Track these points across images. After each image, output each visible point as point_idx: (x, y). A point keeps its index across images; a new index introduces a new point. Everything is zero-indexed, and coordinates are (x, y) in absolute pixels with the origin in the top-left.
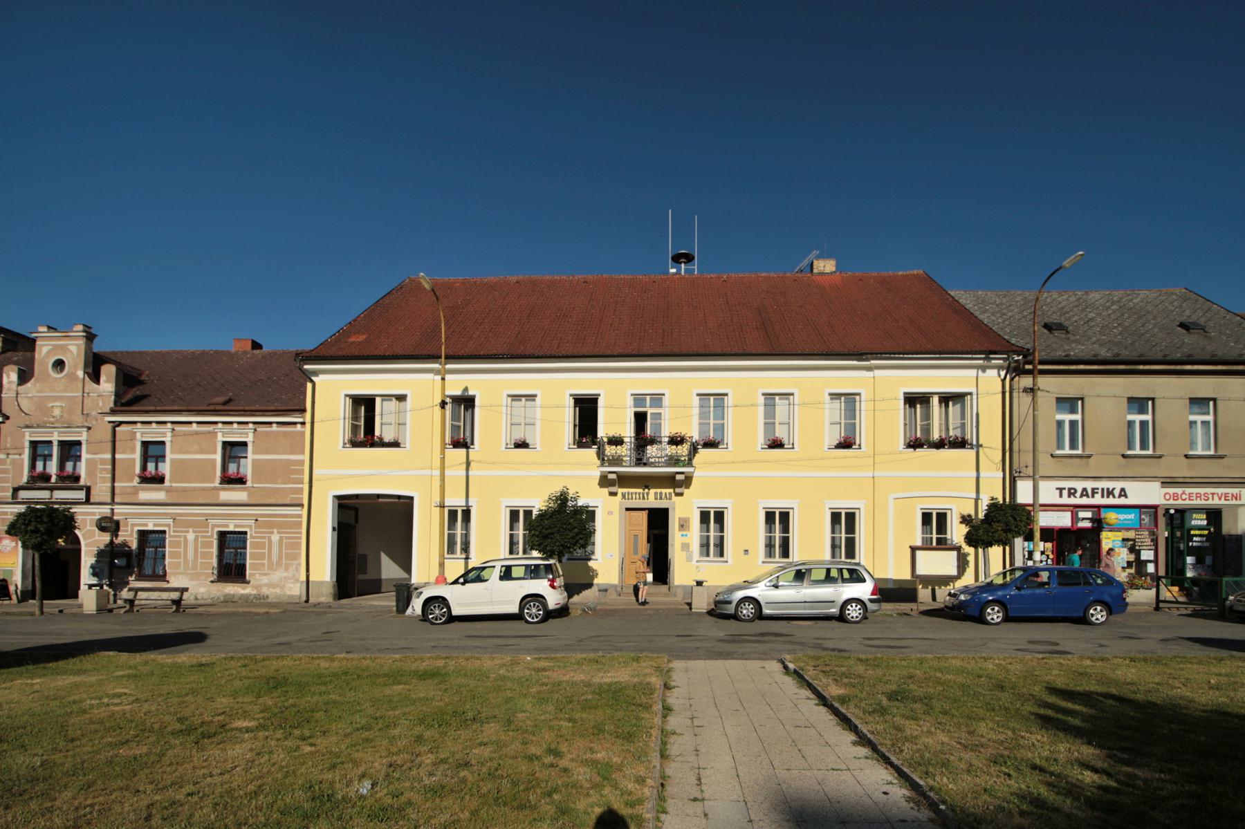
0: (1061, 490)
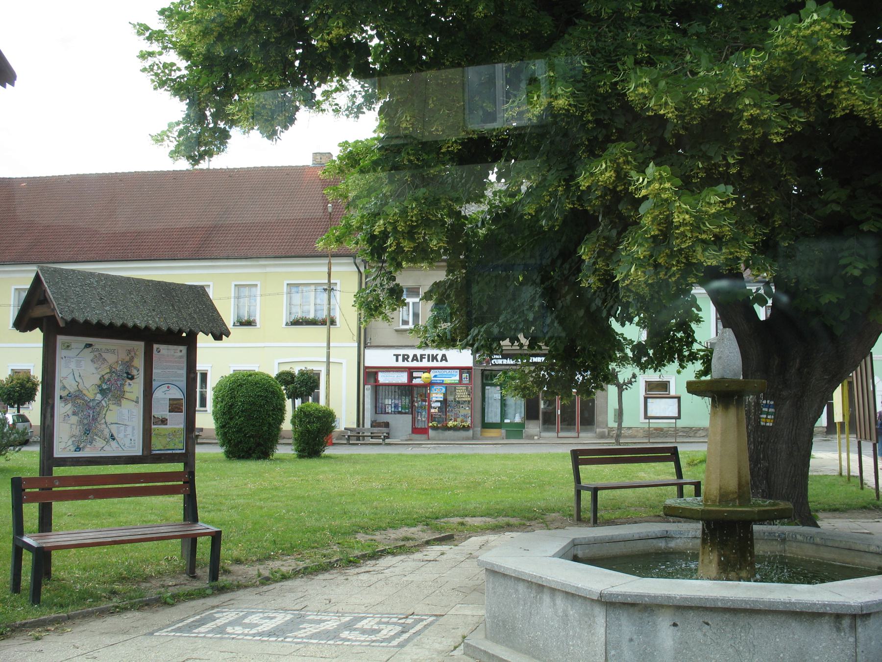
0: (397, 356)
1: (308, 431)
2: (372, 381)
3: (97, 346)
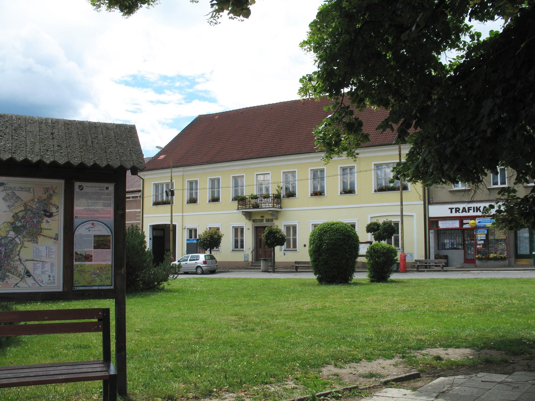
0: (451, 209)
1: (377, 263)
2: (435, 227)
3: (10, 185)
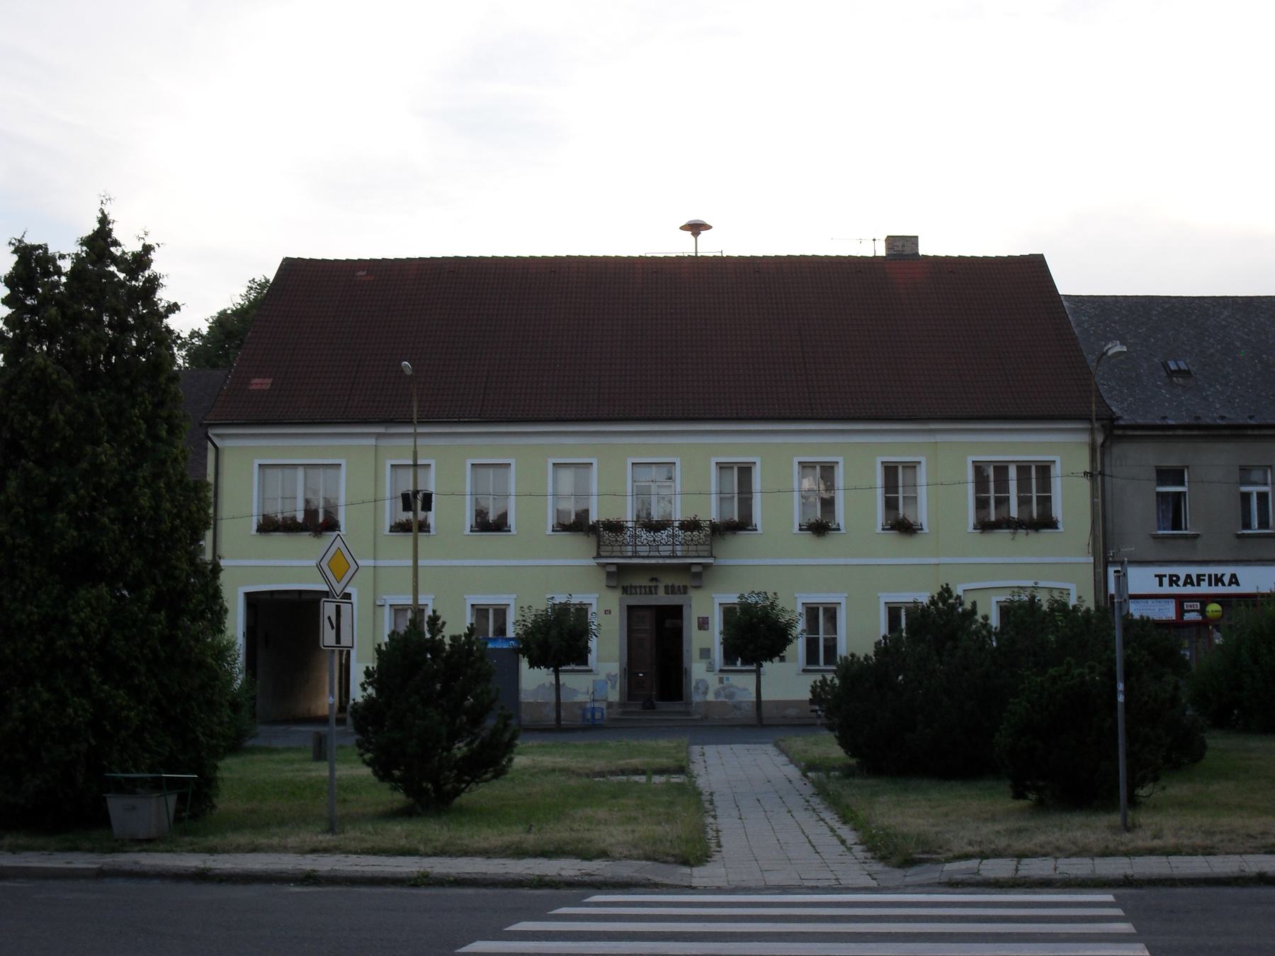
0: (1160, 577)
